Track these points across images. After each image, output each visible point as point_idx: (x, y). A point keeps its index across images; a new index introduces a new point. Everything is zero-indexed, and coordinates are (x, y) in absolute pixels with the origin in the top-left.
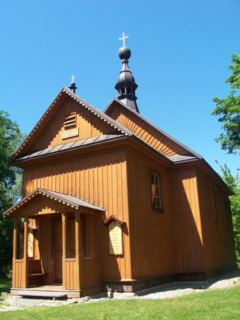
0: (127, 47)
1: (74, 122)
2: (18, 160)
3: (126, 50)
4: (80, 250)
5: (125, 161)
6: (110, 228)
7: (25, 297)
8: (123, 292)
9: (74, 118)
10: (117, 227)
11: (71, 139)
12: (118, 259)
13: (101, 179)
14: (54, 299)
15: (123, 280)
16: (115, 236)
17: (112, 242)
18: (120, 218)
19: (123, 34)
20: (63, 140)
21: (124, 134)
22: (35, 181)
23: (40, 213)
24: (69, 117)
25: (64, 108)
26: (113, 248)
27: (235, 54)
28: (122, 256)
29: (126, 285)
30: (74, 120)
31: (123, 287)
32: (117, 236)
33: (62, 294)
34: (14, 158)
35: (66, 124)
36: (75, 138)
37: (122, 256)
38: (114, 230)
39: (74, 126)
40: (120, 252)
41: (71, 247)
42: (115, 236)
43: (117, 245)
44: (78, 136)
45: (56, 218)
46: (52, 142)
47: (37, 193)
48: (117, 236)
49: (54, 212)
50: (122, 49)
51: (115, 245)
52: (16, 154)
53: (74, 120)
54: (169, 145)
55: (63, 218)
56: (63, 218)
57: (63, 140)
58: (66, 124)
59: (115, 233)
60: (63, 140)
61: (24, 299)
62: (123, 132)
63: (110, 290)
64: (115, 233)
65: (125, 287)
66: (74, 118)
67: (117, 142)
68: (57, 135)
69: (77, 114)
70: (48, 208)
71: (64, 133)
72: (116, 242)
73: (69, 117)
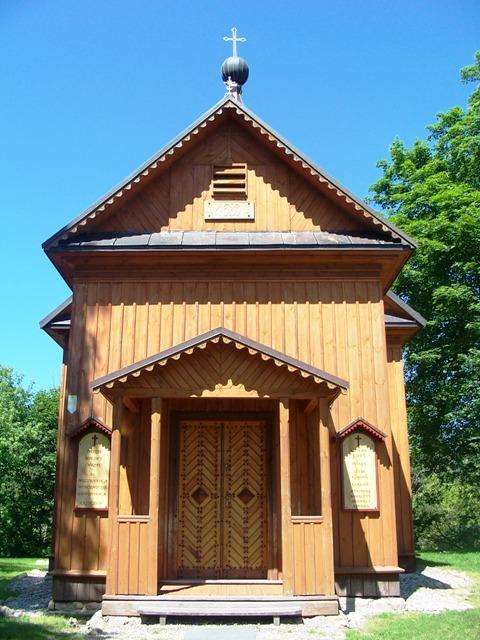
1: (243, 186)
4: (162, 499)
6: (345, 448)
7: (150, 619)
8: (377, 596)
9: (242, 176)
10: (363, 448)
11: (237, 225)
12: (366, 523)
13: (144, 332)
14: (163, 620)
15: (378, 568)
16: (359, 467)
17: (352, 481)
18: (378, 424)
19: (234, 31)
20: (200, 222)
21: (398, 240)
22: (117, 310)
23: (206, 394)
24: (227, 172)
25: (229, 143)
27: (400, 142)
28: (375, 514)
29: (384, 581)
30: (241, 181)
31: (376, 585)
33: (291, 609)
34: (65, 238)
35: (216, 186)
36: (223, 224)
37: (375, 514)
38: (356, 452)
39: (243, 196)
40: (372, 506)
41: (222, 488)
42: (359, 467)
44: (252, 221)
45: (261, 414)
47: (216, 341)
49: (254, 394)
50: (234, 61)
53: (241, 181)
54: (110, 297)
55: (284, 414)
56: (284, 414)
57: (207, 221)
59: (360, 460)
60: (200, 222)
62: (395, 236)
64: (360, 460)
65: (382, 586)
66: (242, 176)
67: (199, 256)
68: (188, 207)
70: (235, 384)
71: (207, 205)
72: (362, 481)
73: (227, 172)
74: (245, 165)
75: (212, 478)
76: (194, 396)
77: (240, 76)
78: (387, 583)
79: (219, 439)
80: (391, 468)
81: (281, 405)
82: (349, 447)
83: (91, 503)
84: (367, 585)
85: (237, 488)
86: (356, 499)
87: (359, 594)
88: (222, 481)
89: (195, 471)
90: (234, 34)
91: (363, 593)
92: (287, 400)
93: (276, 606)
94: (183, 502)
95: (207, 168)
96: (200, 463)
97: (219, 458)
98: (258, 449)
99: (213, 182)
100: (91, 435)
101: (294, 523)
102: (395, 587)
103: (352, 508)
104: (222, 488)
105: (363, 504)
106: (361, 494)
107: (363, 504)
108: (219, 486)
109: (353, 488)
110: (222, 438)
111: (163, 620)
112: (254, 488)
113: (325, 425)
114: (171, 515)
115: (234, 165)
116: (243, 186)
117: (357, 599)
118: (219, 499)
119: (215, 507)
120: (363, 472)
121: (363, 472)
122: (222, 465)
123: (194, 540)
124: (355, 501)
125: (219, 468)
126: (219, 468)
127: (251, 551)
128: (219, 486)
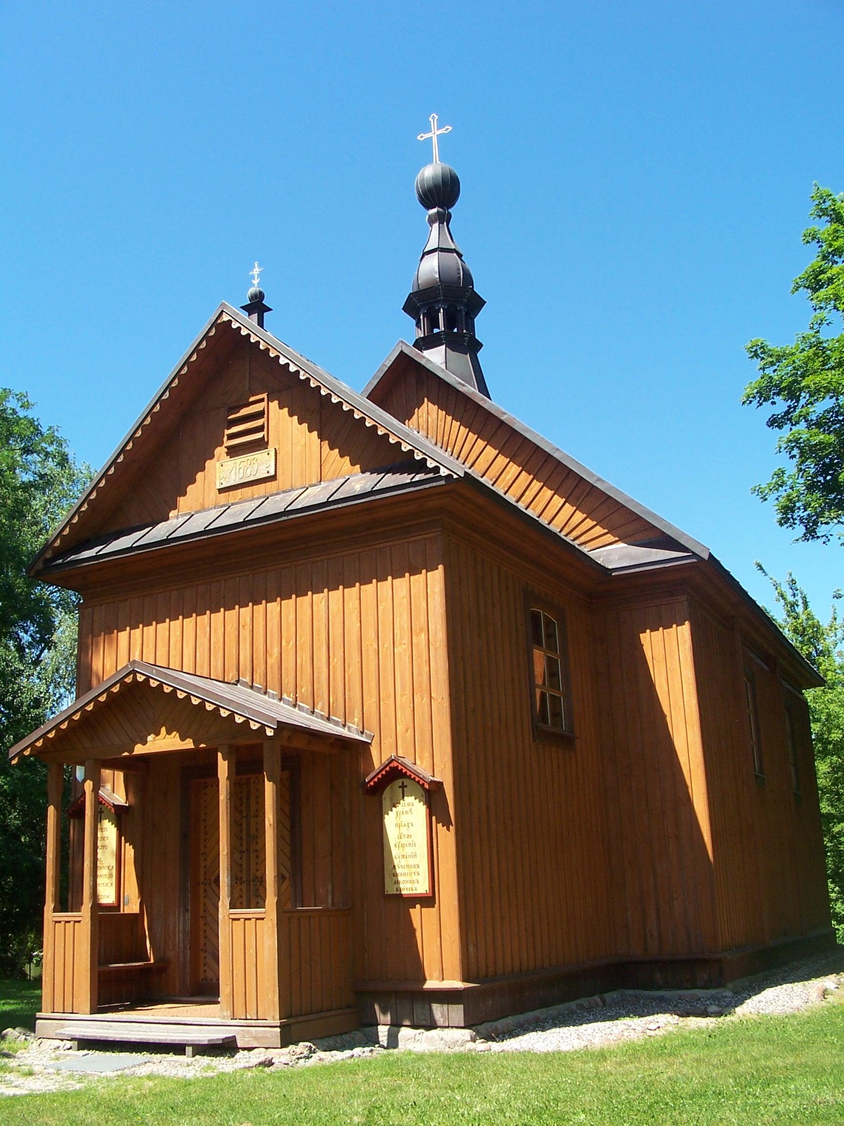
0: (448, 166)
1: (260, 429)
6: (386, 803)
8: (431, 1025)
9: (260, 415)
10: (409, 799)
12: (415, 913)
14: (189, 1050)
15: (431, 984)
16: (404, 830)
17: (395, 852)
18: (422, 768)
20: (219, 494)
21: (436, 470)
22: (123, 636)
23: (139, 749)
24: (244, 412)
25: (224, 381)
26: (398, 871)
27: (825, 190)
28: (428, 901)
32: (419, 878)
34: (48, 555)
35: (231, 437)
37: (428, 901)
38: (400, 808)
39: (261, 444)
40: (422, 887)
41: (249, 870)
42: (404, 830)
43: (411, 861)
44: (273, 478)
47: (128, 680)
49: (189, 744)
50: (430, 172)
51: (403, 862)
52: (58, 543)
55: (223, 767)
56: (223, 767)
57: (221, 491)
58: (231, 437)
59: (404, 819)
60: (219, 494)
62: (431, 464)
64: (404, 819)
65: (438, 1011)
66: (260, 415)
68: (199, 476)
70: (169, 732)
71: (223, 469)
72: (408, 850)
73: (244, 412)
74: (265, 396)
76: (126, 754)
77: (441, 196)
78: (445, 1006)
79: (244, 800)
80: (452, 828)
81: (220, 754)
82: (391, 799)
83: (399, 889)
84: (418, 1009)
86: (400, 878)
87: (407, 1023)
88: (249, 860)
90: (434, 125)
91: (412, 1020)
92: (230, 747)
93: (88, 1027)
94: (205, 891)
97: (244, 826)
99: (227, 432)
100: (399, 782)
101: (233, 919)
102: (457, 1012)
103: (395, 892)
105: (409, 885)
106: (406, 870)
107: (409, 885)
108: (244, 867)
109: (396, 862)
110: (248, 798)
111: (189, 1050)
113: (269, 781)
114: (181, 910)
115: (252, 399)
116: (260, 429)
117: (403, 1029)
118: (244, 885)
119: (241, 897)
120: (409, 836)
121: (409, 836)
124: (397, 882)
125: (244, 843)
126: (244, 843)
128: (244, 867)
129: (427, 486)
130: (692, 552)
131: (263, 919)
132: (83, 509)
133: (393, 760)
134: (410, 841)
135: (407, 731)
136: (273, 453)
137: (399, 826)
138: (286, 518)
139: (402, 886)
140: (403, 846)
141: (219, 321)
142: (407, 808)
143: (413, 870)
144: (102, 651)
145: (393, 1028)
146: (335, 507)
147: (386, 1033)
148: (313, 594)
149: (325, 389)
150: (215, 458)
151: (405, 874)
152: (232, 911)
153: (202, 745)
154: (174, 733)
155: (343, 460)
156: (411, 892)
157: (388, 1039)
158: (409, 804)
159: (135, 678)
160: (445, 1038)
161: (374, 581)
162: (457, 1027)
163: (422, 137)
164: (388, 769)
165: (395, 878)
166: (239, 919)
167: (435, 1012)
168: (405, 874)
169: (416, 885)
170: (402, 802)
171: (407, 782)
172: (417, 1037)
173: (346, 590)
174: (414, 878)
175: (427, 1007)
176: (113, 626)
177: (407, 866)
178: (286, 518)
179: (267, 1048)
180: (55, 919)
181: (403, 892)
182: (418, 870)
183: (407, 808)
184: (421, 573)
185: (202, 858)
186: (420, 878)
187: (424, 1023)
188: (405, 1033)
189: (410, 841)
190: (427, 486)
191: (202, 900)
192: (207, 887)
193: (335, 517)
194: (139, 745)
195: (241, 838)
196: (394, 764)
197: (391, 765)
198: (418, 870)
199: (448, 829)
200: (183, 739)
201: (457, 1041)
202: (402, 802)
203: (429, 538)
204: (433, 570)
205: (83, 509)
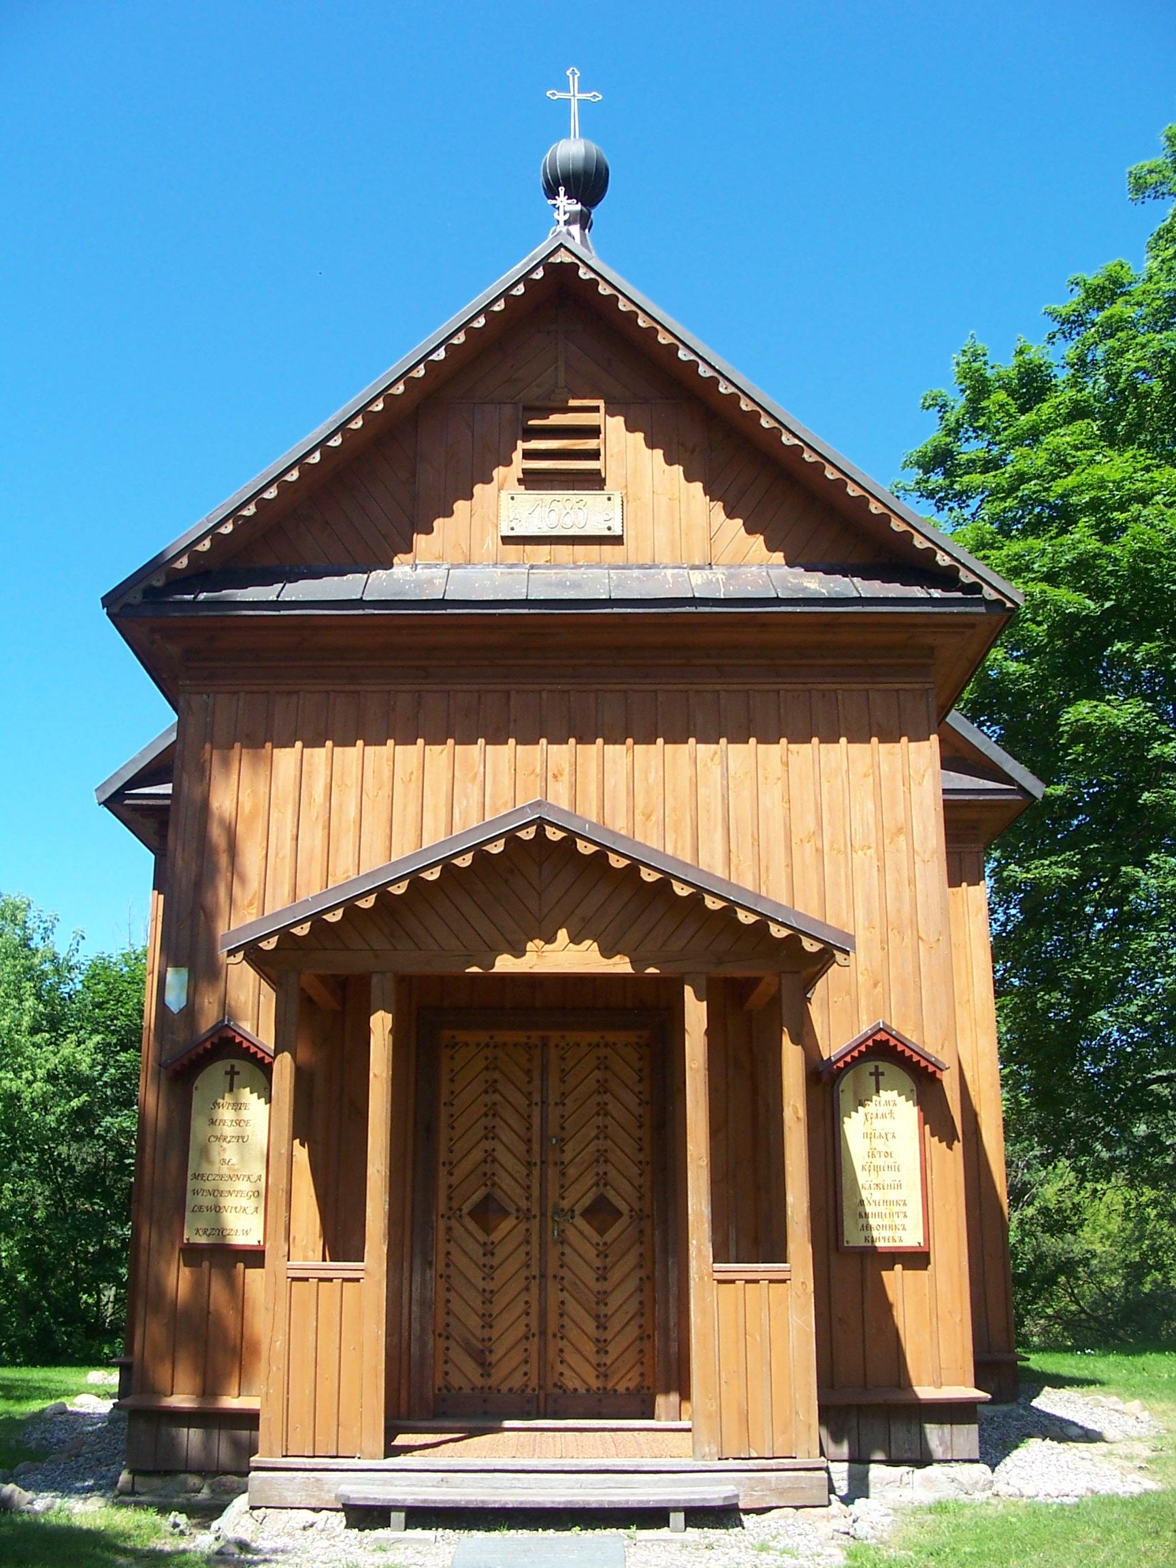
0: (594, 148)
1: (594, 455)
2: (194, 602)
3: (587, 158)
5: (934, 738)
6: (846, 1098)
7: (366, 1516)
8: (923, 1459)
9: (594, 432)
12: (896, 1281)
15: (925, 1392)
16: (879, 1144)
17: (862, 1178)
19: (573, 77)
20: (488, 545)
21: (975, 588)
23: (505, 964)
24: (556, 420)
25: (558, 354)
26: (869, 1209)
27: (981, 346)
28: (917, 1259)
29: (940, 1422)
30: (591, 444)
32: (892, 1145)
33: (712, 1492)
35: (528, 455)
36: (595, 549)
38: (871, 1108)
39: (594, 481)
40: (911, 1238)
41: (543, 1196)
42: (879, 1144)
43: (892, 1195)
44: (617, 540)
46: (420, 540)
47: (528, 835)
48: (892, 1145)
49: (621, 965)
51: (878, 1195)
52: (183, 563)
53: (591, 444)
55: (696, 1013)
56: (696, 1013)
57: (506, 540)
58: (528, 455)
59: (880, 1126)
60: (488, 545)
61: (418, 1533)
63: (844, 1450)
64: (880, 1126)
65: (935, 1435)
66: (594, 432)
68: (460, 506)
69: (610, 412)
70: (575, 939)
71: (506, 503)
72: (887, 1177)
73: (556, 420)
75: (520, 1170)
77: (587, 185)
78: (947, 1428)
79: (536, 1075)
80: (958, 1146)
82: (855, 1094)
84: (899, 1433)
85: (580, 1195)
86: (873, 1222)
87: (879, 1456)
89: (478, 1155)
90: (574, 83)
91: (888, 1452)
95: (508, 410)
96: (490, 1134)
97: (536, 1121)
98: (631, 1100)
99: (521, 445)
102: (967, 1437)
103: (863, 1244)
104: (543, 1196)
106: (882, 1209)
109: (865, 1194)
110: (544, 1069)
111: (398, 1518)
112: (623, 1195)
120: (888, 1154)
121: (888, 1154)
122: (544, 1138)
123: (474, 1322)
124: (868, 1227)
125: (536, 1147)
126: (536, 1147)
127: (614, 1350)
129: (955, 610)
130: (1020, 786)
131: (784, 1281)
132: (246, 513)
133: (881, 1029)
134: (890, 1161)
135: (875, 985)
136: (617, 500)
137: (870, 1136)
138: (693, 609)
139: (875, 1234)
140: (877, 1169)
141: (551, 260)
142: (883, 1109)
143: (896, 1209)
144: (236, 777)
145: (856, 1466)
146: (790, 609)
147: (845, 1475)
148: (335, 745)
149: (769, 419)
150: (495, 484)
151: (880, 1215)
152: (717, 1266)
153: (651, 970)
154: (588, 942)
155: (752, 539)
156: (891, 1244)
157: (849, 1485)
158: (888, 1103)
159: (540, 833)
160: (959, 1477)
161: (299, 744)
162: (965, 1461)
163: (553, 94)
164: (870, 1043)
165: (862, 1221)
166: (733, 1282)
167: (929, 1437)
168: (880, 1215)
169: (900, 1233)
170: (875, 1098)
171: (239, 1064)
172: (905, 1479)
173: (667, 746)
174: (898, 1221)
175: (914, 1429)
176: (262, 735)
177: (885, 1202)
178: (693, 609)
179: (797, 1508)
180: (717, 1276)
181: (877, 1244)
182: (903, 1208)
183: (885, 1110)
184: (506, 743)
185: (442, 1171)
186: (908, 1222)
187: (908, 1455)
188: (877, 1473)
189: (890, 1161)
190: (955, 610)
191: (442, 1246)
192: (454, 1223)
193: (764, 625)
194: (506, 957)
195: (530, 1140)
196: (881, 1037)
197: (878, 1037)
198: (903, 1208)
199: (950, 1147)
200: (607, 953)
201: (976, 1483)
202: (875, 1098)
203: (913, 690)
204: (615, 743)
205: (246, 513)
